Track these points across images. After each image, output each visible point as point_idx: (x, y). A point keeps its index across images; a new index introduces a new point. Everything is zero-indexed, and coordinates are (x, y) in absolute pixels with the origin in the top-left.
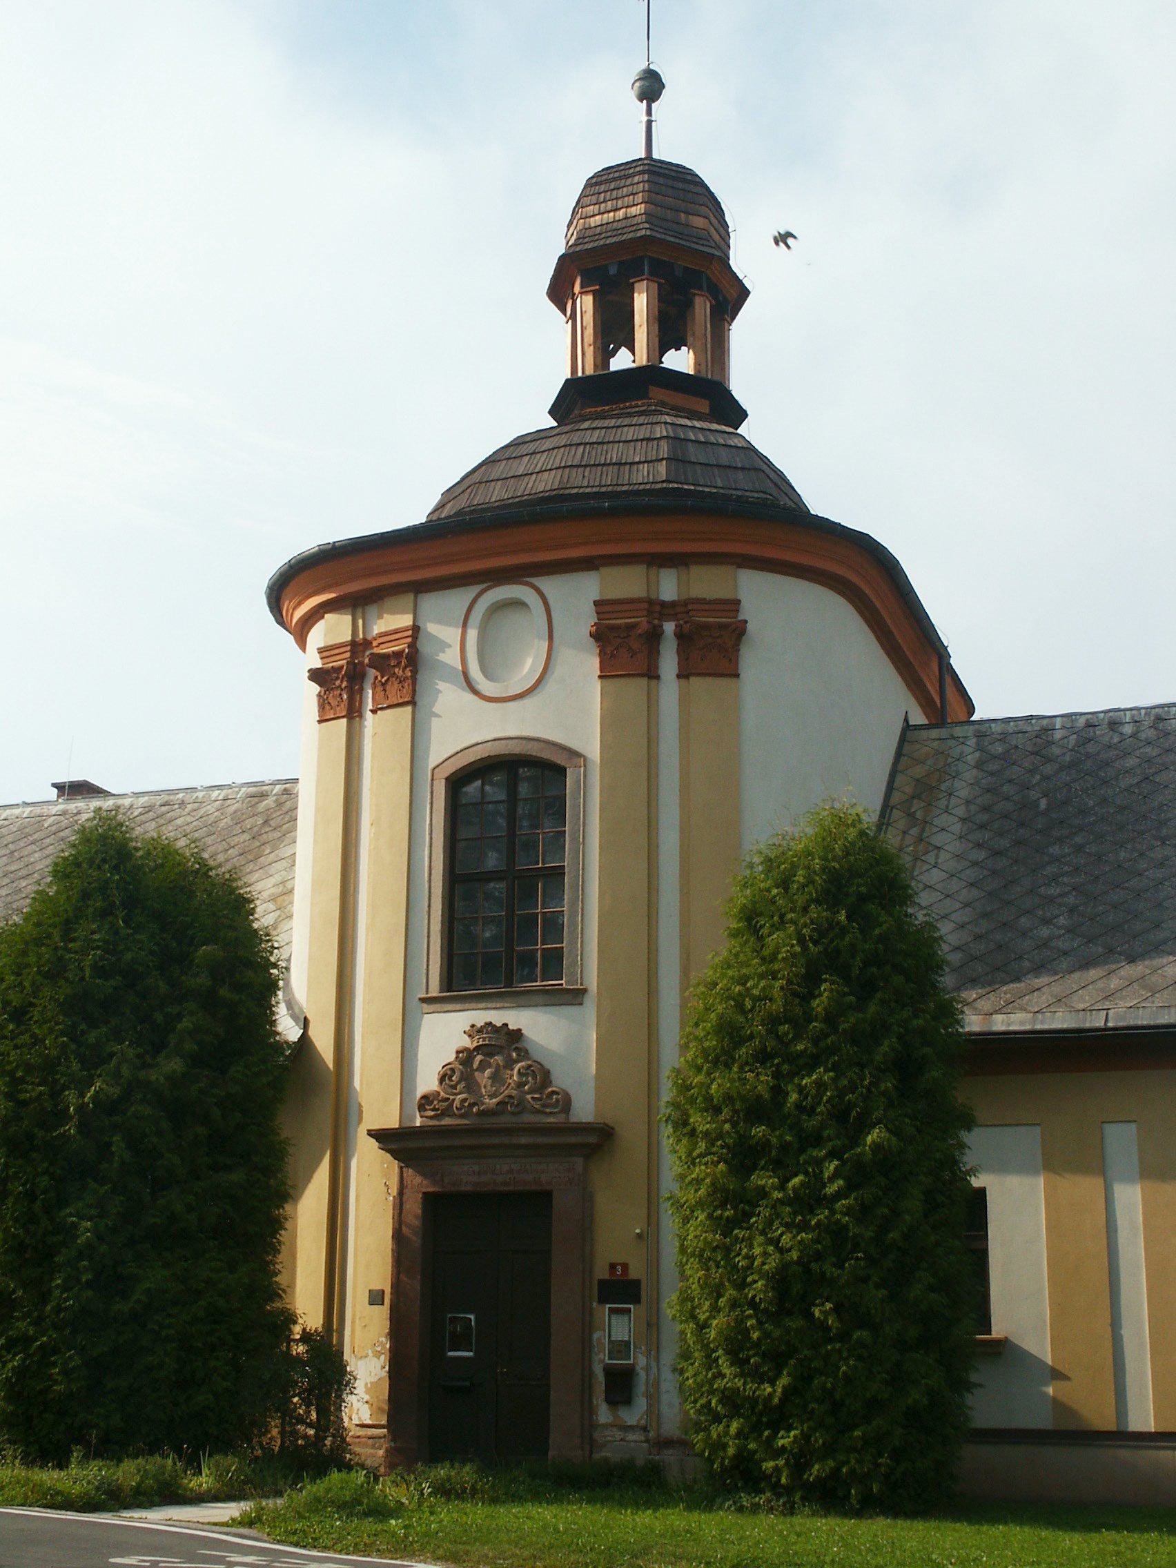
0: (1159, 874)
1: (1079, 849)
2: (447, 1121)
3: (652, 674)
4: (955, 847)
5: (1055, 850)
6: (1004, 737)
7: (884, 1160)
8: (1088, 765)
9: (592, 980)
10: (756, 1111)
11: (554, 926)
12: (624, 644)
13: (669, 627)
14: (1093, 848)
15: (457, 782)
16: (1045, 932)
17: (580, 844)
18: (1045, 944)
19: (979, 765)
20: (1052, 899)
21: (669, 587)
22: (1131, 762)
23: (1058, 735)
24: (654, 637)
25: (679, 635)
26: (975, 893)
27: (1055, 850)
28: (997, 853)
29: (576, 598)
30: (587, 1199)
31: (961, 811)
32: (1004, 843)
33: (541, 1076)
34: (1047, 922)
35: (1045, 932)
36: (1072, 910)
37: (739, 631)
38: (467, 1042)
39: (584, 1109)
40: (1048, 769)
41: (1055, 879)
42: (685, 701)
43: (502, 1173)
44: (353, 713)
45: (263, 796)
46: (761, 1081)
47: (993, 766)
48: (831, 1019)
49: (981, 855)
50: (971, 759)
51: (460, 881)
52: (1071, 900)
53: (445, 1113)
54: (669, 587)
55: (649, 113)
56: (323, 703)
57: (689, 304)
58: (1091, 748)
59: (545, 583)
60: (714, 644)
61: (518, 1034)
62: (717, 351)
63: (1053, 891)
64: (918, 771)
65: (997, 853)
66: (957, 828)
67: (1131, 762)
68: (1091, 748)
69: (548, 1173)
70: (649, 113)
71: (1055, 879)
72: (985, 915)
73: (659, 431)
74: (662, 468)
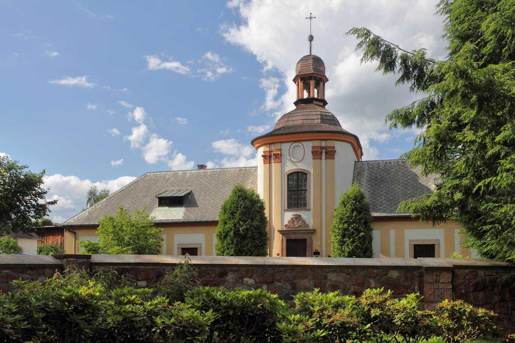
0: (398, 191)
1: (386, 186)
2: (290, 229)
3: (321, 159)
4: (365, 184)
5: (382, 186)
6: (372, 164)
7: (363, 237)
8: (386, 170)
9: (312, 207)
10: (346, 230)
11: (305, 199)
12: (316, 154)
13: (324, 151)
14: (388, 186)
15: (288, 175)
16: (381, 200)
17: (310, 186)
18: (381, 202)
19: (368, 169)
20: (382, 195)
21: (323, 144)
22: (393, 170)
23: (381, 164)
24: (322, 152)
25: (326, 152)
26: (369, 193)
27: (382, 186)
28: (372, 186)
29: (309, 146)
30: (312, 240)
31: (366, 178)
32: (373, 184)
33: (304, 222)
34: (381, 198)
35: (381, 200)
36: (385, 196)
37: (335, 152)
38: (292, 217)
39: (311, 227)
40: (380, 171)
41: (382, 191)
42: (326, 163)
43: (299, 236)
44: (270, 163)
45: (241, 170)
46: (346, 225)
47: (371, 170)
48: (356, 216)
49: (370, 186)
50: (367, 168)
51: (290, 190)
52: (385, 195)
53: (289, 227)
54: (323, 144)
55: (311, 44)
56: (264, 161)
57: (320, 84)
58: (387, 167)
59: (303, 143)
60: (331, 154)
61: (300, 216)
62: (322, 92)
63: (382, 193)
64: (358, 170)
65: (372, 186)
66: (365, 181)
67: (393, 170)
68: (387, 167)
69: (306, 236)
70: (311, 44)
71: (382, 191)
72: (371, 197)
73: (319, 113)
74: (319, 120)
